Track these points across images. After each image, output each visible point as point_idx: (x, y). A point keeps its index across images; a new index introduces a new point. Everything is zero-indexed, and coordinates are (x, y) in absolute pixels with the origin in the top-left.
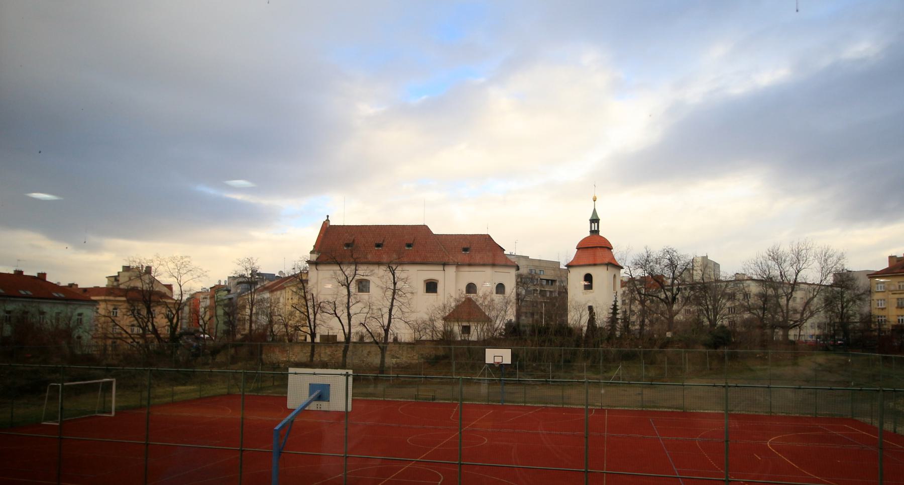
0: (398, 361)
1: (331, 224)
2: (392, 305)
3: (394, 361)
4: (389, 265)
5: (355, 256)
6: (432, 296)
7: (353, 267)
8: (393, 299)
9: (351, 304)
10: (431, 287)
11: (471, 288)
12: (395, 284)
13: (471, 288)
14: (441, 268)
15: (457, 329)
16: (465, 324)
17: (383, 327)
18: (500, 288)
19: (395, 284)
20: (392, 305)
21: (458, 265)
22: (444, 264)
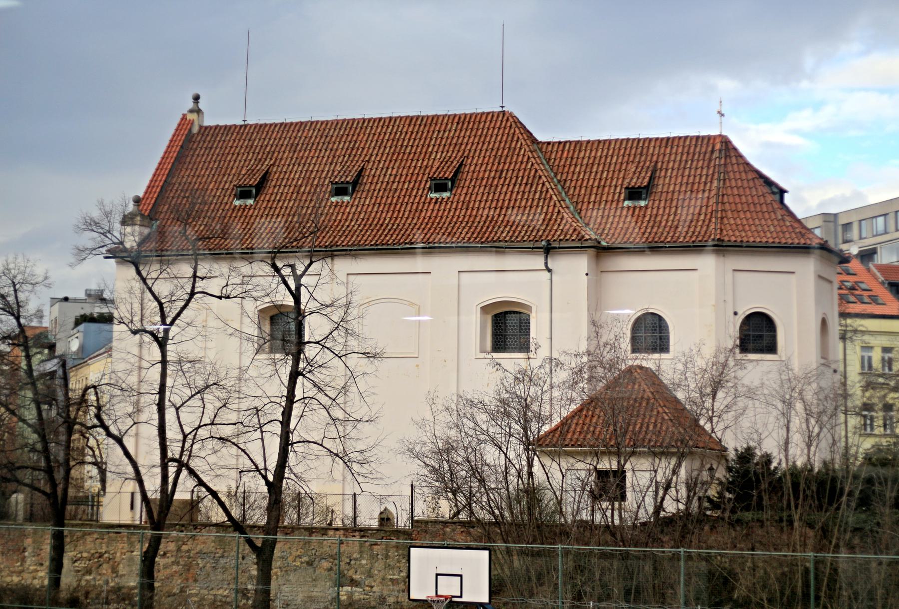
0: (358, 593)
6: (512, 360)
10: (507, 327)
11: (652, 332)
14: (537, 261)
16: (607, 464)
18: (758, 333)
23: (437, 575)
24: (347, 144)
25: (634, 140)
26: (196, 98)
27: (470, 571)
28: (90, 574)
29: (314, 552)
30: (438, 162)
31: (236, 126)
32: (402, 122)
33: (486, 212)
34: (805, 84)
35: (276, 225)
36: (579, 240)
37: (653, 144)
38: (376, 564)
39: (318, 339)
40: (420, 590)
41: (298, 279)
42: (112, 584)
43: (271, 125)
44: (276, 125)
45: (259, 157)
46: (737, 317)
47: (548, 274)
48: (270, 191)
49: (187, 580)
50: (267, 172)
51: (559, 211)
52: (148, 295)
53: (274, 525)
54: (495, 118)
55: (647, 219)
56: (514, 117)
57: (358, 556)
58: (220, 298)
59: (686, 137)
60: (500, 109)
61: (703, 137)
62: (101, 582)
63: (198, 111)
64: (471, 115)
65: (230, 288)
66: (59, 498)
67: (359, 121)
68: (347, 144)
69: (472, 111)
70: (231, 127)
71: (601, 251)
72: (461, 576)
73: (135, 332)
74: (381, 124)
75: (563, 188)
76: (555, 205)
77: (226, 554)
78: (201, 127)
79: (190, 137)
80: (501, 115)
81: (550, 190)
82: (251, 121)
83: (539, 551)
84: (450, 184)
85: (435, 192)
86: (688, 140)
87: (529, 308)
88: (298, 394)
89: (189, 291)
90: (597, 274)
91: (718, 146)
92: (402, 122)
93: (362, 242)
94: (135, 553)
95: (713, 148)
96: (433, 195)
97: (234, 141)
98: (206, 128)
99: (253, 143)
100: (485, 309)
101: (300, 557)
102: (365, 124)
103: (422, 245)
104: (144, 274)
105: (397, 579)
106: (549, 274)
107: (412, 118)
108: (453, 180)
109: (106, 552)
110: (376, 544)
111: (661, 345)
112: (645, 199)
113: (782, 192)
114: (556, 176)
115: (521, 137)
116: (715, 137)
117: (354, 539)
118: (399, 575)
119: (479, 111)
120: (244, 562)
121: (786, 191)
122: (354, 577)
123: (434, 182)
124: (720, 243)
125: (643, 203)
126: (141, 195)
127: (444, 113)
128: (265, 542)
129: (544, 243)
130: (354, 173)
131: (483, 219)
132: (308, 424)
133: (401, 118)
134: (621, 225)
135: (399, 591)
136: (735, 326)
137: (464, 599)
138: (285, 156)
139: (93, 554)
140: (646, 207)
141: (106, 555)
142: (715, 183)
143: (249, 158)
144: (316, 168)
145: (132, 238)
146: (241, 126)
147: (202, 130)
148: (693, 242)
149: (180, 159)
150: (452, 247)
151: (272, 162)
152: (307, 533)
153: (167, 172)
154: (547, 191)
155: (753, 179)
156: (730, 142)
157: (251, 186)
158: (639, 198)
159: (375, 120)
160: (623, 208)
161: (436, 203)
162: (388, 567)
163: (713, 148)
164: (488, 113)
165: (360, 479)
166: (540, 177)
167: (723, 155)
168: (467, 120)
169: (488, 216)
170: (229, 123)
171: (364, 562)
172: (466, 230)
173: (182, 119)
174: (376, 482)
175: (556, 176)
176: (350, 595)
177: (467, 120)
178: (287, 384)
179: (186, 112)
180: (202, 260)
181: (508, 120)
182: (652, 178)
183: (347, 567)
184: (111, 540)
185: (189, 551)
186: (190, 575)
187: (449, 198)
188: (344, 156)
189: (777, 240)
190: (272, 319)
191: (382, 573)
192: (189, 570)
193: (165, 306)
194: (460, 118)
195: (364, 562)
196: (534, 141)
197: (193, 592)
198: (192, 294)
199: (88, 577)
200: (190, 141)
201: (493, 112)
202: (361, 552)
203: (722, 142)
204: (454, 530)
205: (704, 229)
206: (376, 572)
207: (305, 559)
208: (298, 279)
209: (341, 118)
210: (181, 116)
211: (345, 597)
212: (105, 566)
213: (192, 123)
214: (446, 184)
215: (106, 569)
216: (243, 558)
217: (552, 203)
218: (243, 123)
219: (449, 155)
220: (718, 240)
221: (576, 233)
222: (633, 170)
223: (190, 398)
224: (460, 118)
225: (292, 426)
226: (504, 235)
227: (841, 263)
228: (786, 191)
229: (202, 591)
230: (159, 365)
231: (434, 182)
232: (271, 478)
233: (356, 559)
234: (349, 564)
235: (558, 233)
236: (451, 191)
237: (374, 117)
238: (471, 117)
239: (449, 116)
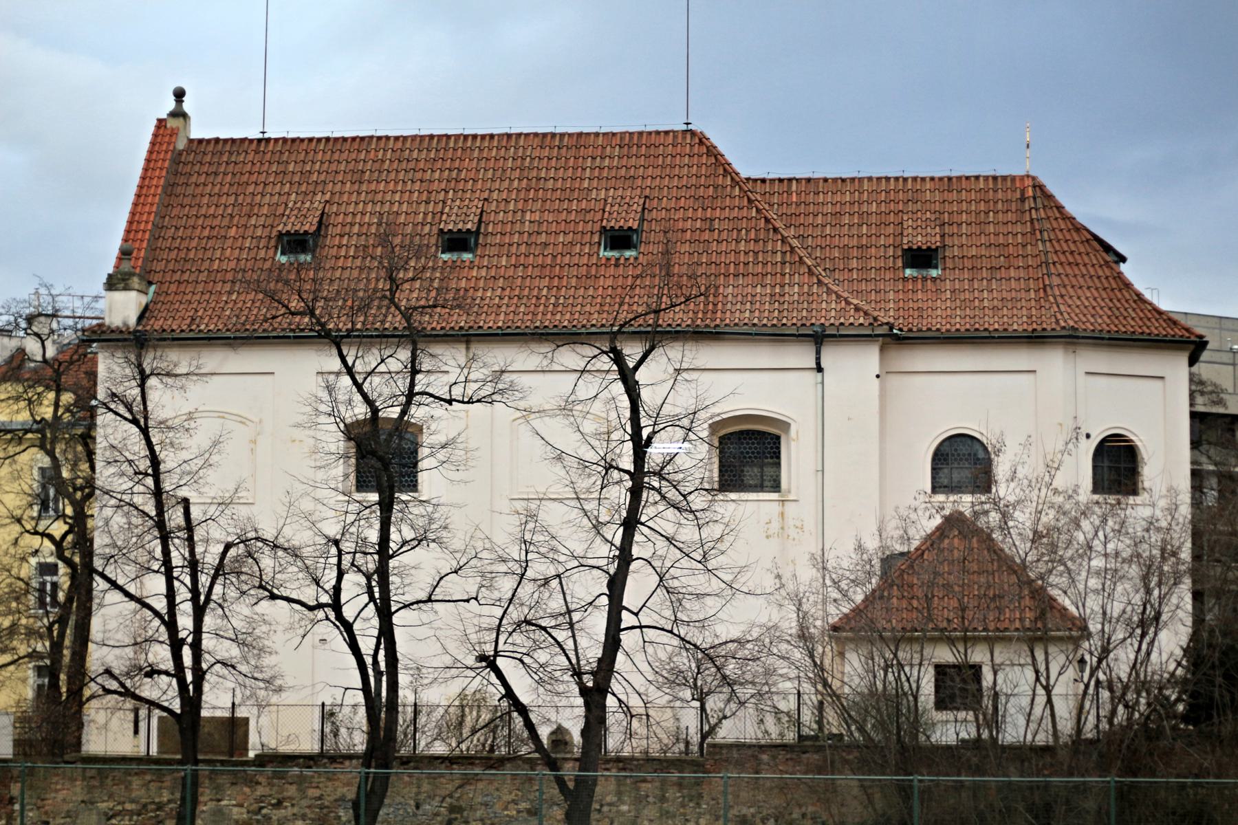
1: (199, 130)
2: (625, 557)
4: (610, 340)
5: (409, 296)
8: (631, 524)
11: (962, 461)
12: (640, 447)
13: (962, 461)
14: (802, 356)
17: (577, 673)
18: (1117, 464)
19: (640, 447)
20: (625, 557)
21: (894, 339)
22: (819, 338)
26: (179, 95)
38: (646, 812)
57: (615, 799)
58: (450, 402)
60: (684, 127)
63: (184, 116)
66: (382, 724)
82: (272, 134)
85: (613, 248)
91: (1030, 192)
101: (515, 802)
110: (644, 781)
111: (983, 480)
112: (936, 267)
120: (420, 812)
125: (934, 273)
128: (578, 780)
139: (145, 806)
146: (259, 141)
149: (170, 189)
150: (289, 337)
152: (527, 766)
171: (625, 808)
179: (165, 116)
185: (320, 798)
195: (625, 808)
202: (619, 794)
203: (1034, 187)
207: (523, 805)
213: (174, 133)
216: (418, 807)
218: (260, 136)
233: (610, 804)
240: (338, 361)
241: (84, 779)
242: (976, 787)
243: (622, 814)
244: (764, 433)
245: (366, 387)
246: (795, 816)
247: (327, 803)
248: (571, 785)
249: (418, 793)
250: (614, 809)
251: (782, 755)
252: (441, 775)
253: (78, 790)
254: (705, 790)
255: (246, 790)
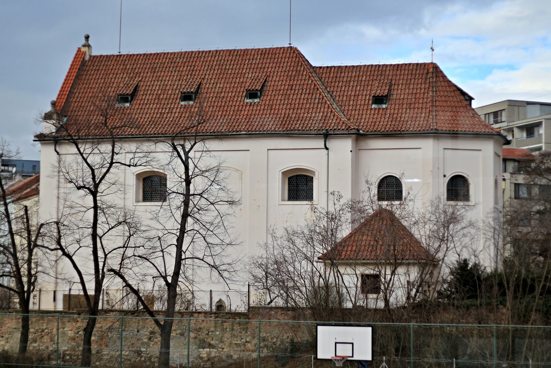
0: (214, 353)
2: (183, 230)
3: (204, 353)
6: (302, 206)
7: (106, 148)
9: (99, 232)
10: (299, 185)
11: (390, 188)
12: (188, 181)
14: (320, 143)
15: (350, 279)
16: (369, 271)
18: (457, 188)
19: (188, 181)
20: (183, 230)
23: (336, 343)
24: (189, 68)
25: (376, 65)
26: (87, 38)
27: (359, 341)
28: (36, 342)
29: (184, 327)
30: (251, 80)
31: (114, 56)
32: (225, 54)
33: (284, 111)
34: (423, 32)
35: (146, 120)
36: (347, 129)
37: (388, 68)
38: (226, 335)
39: (199, 192)
40: (324, 352)
41: (186, 153)
42: (51, 349)
43: (137, 55)
44: (141, 55)
45: (131, 76)
46: (445, 178)
47: (326, 151)
48: (140, 98)
49: (101, 345)
50: (137, 86)
51: (332, 111)
52: (85, 165)
53: (170, 312)
54: (285, 51)
55: (388, 116)
56: (298, 51)
57: (214, 329)
58: (129, 166)
59: (410, 64)
60: (289, 46)
61: (421, 64)
62: (43, 347)
63: (89, 46)
64: (270, 49)
65: (136, 160)
67: (196, 52)
68: (189, 68)
69: (270, 47)
70: (111, 56)
71: (360, 136)
72: (352, 344)
73: (79, 188)
74: (211, 54)
75: (331, 96)
76: (328, 107)
77: (126, 329)
78: (90, 56)
79: (84, 63)
80: (290, 49)
81: (325, 97)
82: (123, 53)
83: (398, 327)
84: (259, 93)
85: (250, 98)
86: (412, 65)
87: (313, 172)
88: (188, 227)
89: (109, 161)
90: (356, 151)
91: (431, 70)
92: (225, 54)
93: (149, 132)
94: (66, 329)
95: (428, 71)
96: (248, 101)
97: (114, 65)
98: (94, 57)
99: (126, 67)
100: (284, 173)
102: (200, 55)
103: (244, 132)
104: (82, 151)
105: (239, 344)
106: (326, 151)
107: (231, 51)
108: (261, 91)
109: (46, 328)
110: (225, 322)
112: (385, 104)
113: (471, 99)
114: (326, 88)
115: (303, 63)
116: (429, 64)
117: (211, 319)
118: (241, 341)
119: (183, 51)
120: (139, 334)
121: (473, 99)
122: (211, 342)
123: (248, 92)
124: (436, 132)
125: (384, 106)
126: (55, 99)
127: (251, 48)
128: (165, 321)
129: (324, 131)
130: (132, 89)
131: (282, 116)
132: (193, 247)
133: (224, 51)
134: (371, 120)
135: (241, 351)
136: (444, 185)
137: (355, 358)
138: (148, 75)
139: (37, 330)
140: (386, 108)
141: (46, 331)
142: (431, 94)
143: (124, 76)
144: (169, 83)
145: (49, 128)
146: (118, 56)
147: (92, 58)
148: (419, 131)
149: (78, 77)
151: (140, 79)
152: (180, 316)
153: (70, 86)
154: (323, 98)
155: (454, 91)
156: (438, 67)
157: (127, 94)
158: (382, 103)
159: (206, 52)
160: (371, 109)
161: (250, 105)
162: (233, 336)
163: (428, 71)
164: (281, 48)
165: (228, 282)
166: (318, 89)
167: (435, 76)
168: (267, 52)
169: (285, 114)
170: (109, 53)
171: (217, 333)
172: (272, 123)
173: (78, 51)
174: (238, 283)
175: (326, 88)
176: (209, 354)
177: (267, 52)
178: (180, 222)
179: (80, 46)
180: (117, 141)
181: (294, 52)
182: (390, 90)
183: (207, 336)
184: (49, 321)
185: (101, 327)
186: (103, 343)
187: (259, 103)
188: (188, 75)
189: (472, 130)
190: (144, 180)
191: (229, 340)
192: (102, 339)
193: (96, 171)
194: (262, 51)
195: (217, 333)
196: (311, 66)
197: (105, 353)
198: (112, 163)
199: (35, 345)
200: (84, 66)
201: (284, 47)
202: (215, 327)
203: (433, 67)
204: (276, 313)
205: (425, 122)
206: (226, 339)
208: (186, 153)
209: (183, 50)
210: (77, 49)
211: (206, 355)
212: (46, 337)
213: (84, 53)
214: (257, 94)
215: (46, 339)
216: (138, 331)
217: (327, 106)
218: (118, 54)
219: (257, 75)
220: (436, 129)
221: (345, 125)
222: (377, 85)
223: (108, 231)
224: (262, 51)
225: (184, 248)
226: (297, 126)
227: (505, 144)
228: (473, 99)
229: (111, 353)
230: (92, 210)
231: (248, 92)
232: (169, 280)
233: (212, 332)
234: (208, 334)
235: (333, 125)
236: (260, 98)
237: (206, 50)
238: (181, 54)
239: (255, 50)
240: (77, 150)
241: (16, 319)
242: (457, 327)
243: (217, 335)
244: (307, 176)
245: (88, 160)
246: (284, 337)
247: (104, 330)
248: (162, 323)
249: (138, 326)
250: (214, 333)
251: (280, 312)
252: (147, 319)
253: (14, 323)
254: (249, 326)
255: (74, 324)
